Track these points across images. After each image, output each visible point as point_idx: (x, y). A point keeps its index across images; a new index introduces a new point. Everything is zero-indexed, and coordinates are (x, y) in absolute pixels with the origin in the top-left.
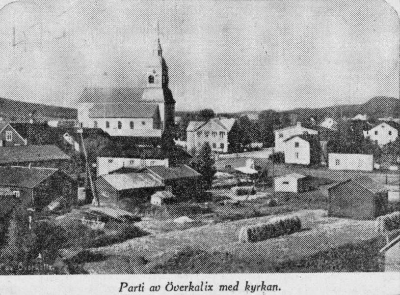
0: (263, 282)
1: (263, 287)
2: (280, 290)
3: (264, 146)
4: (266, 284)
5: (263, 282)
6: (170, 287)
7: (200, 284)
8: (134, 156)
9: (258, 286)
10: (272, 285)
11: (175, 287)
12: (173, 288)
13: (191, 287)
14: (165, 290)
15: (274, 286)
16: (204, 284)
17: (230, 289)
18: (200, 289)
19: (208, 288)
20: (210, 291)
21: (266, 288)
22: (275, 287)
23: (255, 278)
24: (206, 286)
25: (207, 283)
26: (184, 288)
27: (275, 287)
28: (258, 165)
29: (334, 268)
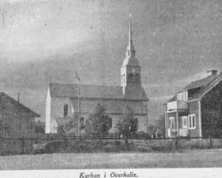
0: (92, 173)
1: (92, 175)
2: (214, 175)
3: (192, 98)
4: (93, 174)
5: (92, 173)
6: (113, 175)
7: (130, 173)
8: (203, 111)
9: (89, 175)
10: (97, 174)
11: (116, 175)
12: (115, 175)
13: (125, 175)
14: (110, 177)
15: (98, 175)
16: (132, 173)
17: (120, 176)
18: (130, 176)
19: (133, 175)
20: (135, 177)
21: (126, 176)
22: (98, 176)
23: (128, 171)
24: (132, 175)
25: (133, 172)
26: (121, 176)
27: (98, 176)
28: (54, 81)
29: (180, 166)
